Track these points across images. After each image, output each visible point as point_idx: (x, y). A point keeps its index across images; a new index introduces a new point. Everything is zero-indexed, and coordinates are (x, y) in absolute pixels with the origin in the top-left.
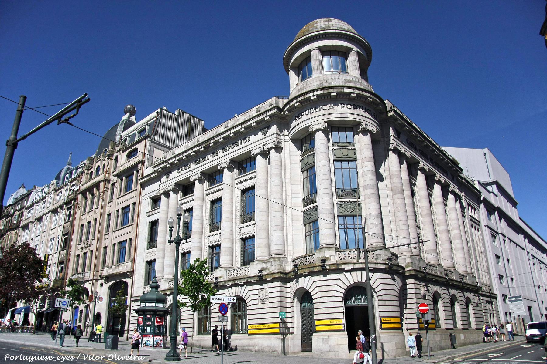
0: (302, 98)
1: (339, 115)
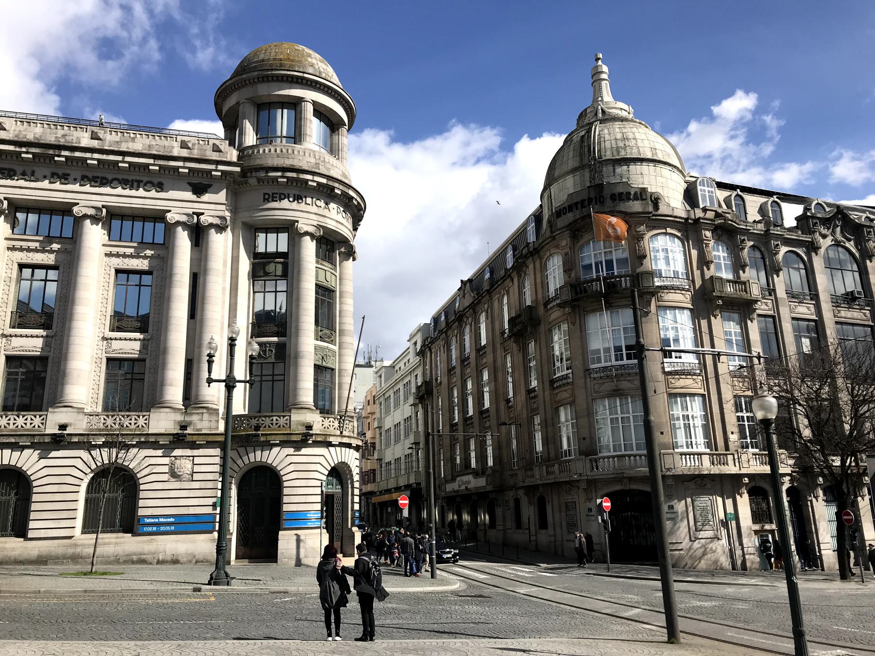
0: (294, 175)
1: (334, 223)
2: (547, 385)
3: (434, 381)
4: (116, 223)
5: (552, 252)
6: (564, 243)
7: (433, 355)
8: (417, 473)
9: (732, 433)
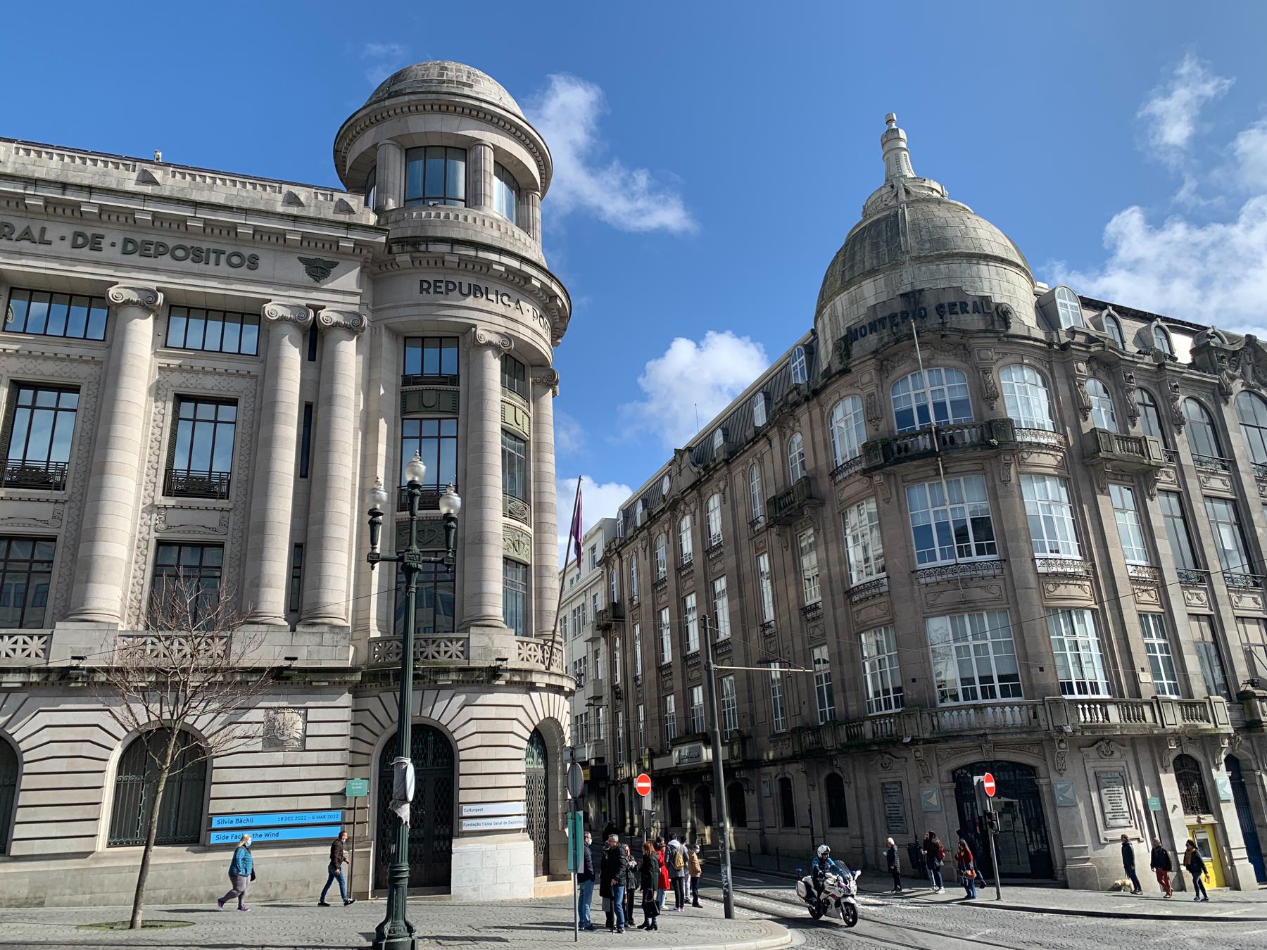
1: (529, 333)
2: (840, 598)
3: (627, 603)
4: (178, 323)
5: (842, 395)
6: (866, 379)
7: (625, 564)
8: (598, 743)
9: (1143, 670)
